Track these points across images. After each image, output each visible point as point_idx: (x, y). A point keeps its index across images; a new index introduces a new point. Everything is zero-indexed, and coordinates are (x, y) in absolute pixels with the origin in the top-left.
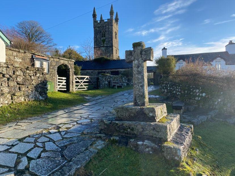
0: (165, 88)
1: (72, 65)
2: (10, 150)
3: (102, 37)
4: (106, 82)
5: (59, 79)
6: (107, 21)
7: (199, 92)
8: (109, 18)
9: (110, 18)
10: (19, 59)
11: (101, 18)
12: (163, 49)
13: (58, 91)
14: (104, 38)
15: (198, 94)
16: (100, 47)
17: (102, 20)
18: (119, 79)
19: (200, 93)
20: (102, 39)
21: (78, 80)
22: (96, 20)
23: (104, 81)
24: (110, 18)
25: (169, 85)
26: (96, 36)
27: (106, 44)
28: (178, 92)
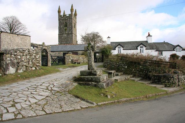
3: (65, 27)
6: (68, 15)
11: (64, 13)
14: (66, 28)
17: (64, 15)
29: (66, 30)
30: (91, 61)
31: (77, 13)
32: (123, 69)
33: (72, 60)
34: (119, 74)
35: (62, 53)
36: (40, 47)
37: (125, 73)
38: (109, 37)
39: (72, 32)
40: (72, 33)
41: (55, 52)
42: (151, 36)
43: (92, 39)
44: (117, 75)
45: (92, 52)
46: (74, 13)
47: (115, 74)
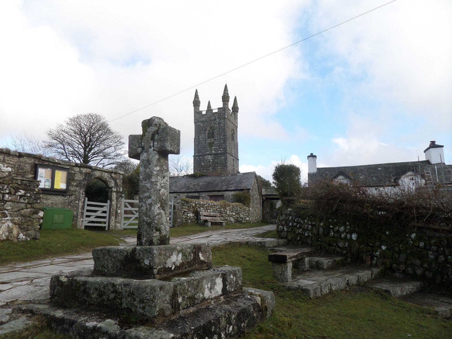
0: (283, 223)
1: (118, 181)
4: (189, 215)
5: (88, 205)
6: (217, 111)
7: (345, 231)
8: (221, 105)
10: (7, 167)
11: (209, 106)
12: (308, 157)
13: (86, 227)
15: (343, 236)
16: (204, 156)
18: (218, 208)
19: (347, 233)
20: (208, 141)
21: (130, 208)
23: (185, 212)
25: (290, 218)
26: (198, 137)
27: (216, 150)
29: (211, 145)
30: (149, 201)
31: (239, 105)
32: (341, 244)
34: (326, 261)
37: (352, 260)
39: (225, 149)
40: (225, 153)
44: (317, 267)
45: (154, 162)
46: (231, 105)
47: (310, 262)
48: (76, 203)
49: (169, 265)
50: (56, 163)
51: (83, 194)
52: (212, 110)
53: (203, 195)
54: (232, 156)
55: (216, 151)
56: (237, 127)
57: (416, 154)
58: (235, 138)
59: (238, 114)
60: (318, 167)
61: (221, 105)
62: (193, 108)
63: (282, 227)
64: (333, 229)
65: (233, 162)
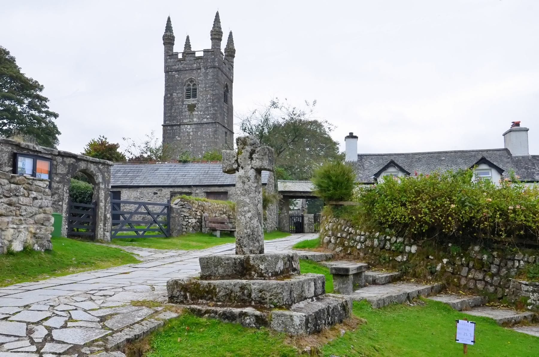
0: (330, 233)
2: (137, 206)
3: (188, 97)
4: (190, 221)
6: (201, 54)
8: (208, 45)
9: (210, 48)
11: (188, 45)
12: (347, 137)
14: (192, 101)
17: (188, 51)
22: (172, 50)
23: (185, 216)
24: (210, 48)
26: (171, 95)
28: (360, 244)
29: (192, 108)
31: (236, 46)
33: (200, 221)
35: (167, 192)
36: (63, 163)
38: (352, 136)
41: (140, 190)
42: (527, 130)
43: (294, 140)
48: (60, 205)
49: (277, 270)
50: (37, 151)
51: (66, 192)
52: (194, 53)
53: (197, 192)
54: (224, 127)
55: (199, 118)
56: (232, 82)
57: (493, 141)
58: (229, 99)
59: (235, 60)
60: (358, 153)
61: (208, 45)
62: (162, 48)
63: (328, 238)
64: (389, 240)
65: (226, 136)
